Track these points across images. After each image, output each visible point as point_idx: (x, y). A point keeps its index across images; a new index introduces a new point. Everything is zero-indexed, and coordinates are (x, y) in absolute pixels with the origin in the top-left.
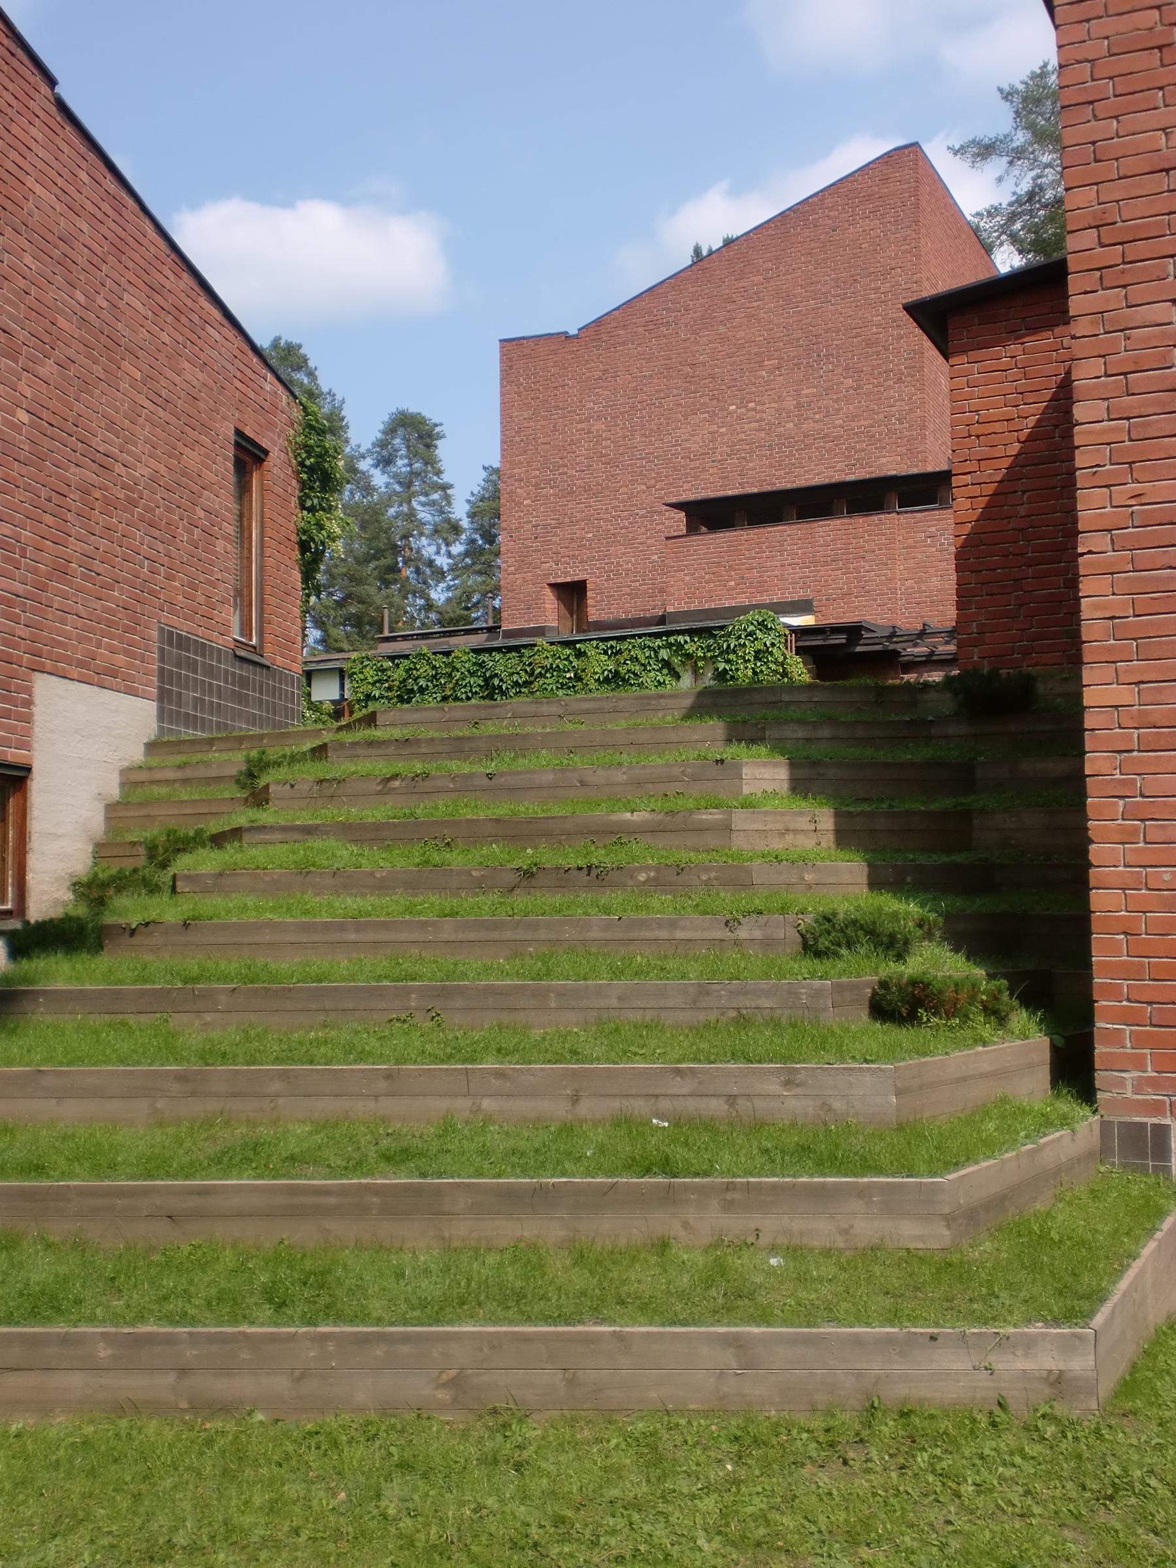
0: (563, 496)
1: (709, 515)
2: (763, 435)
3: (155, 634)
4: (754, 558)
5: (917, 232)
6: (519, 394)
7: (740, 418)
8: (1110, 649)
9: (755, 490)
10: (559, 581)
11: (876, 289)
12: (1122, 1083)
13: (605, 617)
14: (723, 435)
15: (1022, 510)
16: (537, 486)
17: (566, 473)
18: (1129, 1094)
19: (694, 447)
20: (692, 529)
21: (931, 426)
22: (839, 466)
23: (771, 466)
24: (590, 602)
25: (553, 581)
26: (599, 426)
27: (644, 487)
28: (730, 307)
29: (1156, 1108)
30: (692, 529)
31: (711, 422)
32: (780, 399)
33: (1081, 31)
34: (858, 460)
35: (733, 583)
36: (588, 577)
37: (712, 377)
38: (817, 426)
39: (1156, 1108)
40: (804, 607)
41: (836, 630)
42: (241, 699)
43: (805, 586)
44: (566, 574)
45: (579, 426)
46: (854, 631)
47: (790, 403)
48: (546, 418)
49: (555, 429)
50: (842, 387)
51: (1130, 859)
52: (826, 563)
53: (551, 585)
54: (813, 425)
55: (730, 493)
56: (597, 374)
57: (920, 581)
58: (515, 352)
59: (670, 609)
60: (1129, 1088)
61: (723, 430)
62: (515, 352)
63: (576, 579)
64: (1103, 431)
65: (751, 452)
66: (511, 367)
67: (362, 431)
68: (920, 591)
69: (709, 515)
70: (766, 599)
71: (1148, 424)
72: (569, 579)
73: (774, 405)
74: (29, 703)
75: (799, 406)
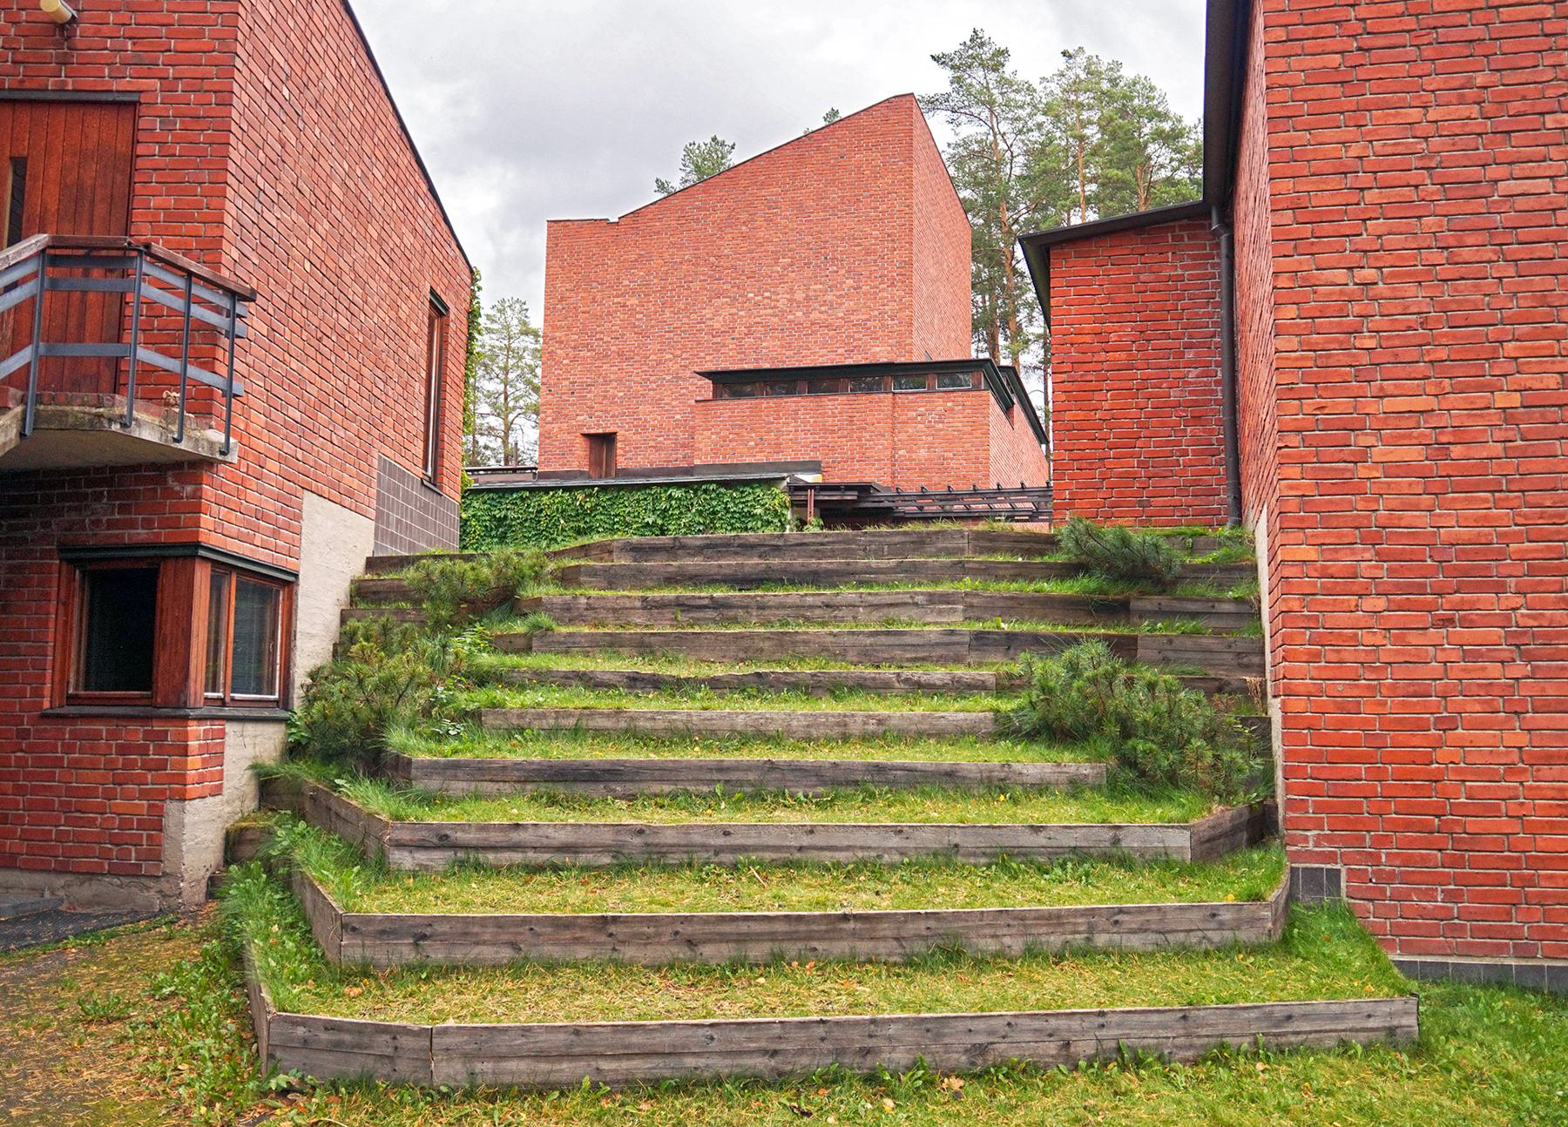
1: (731, 383)
2: (776, 320)
3: (376, 462)
5: (911, 165)
6: (563, 268)
7: (757, 304)
8: (1302, 519)
9: (767, 366)
12: (1306, 839)
13: (632, 465)
15: (1106, 405)
16: (574, 348)
18: (1311, 846)
19: (717, 326)
20: (717, 395)
21: (916, 324)
22: (840, 351)
23: (782, 347)
24: (619, 452)
25: (586, 431)
26: (634, 301)
29: (1331, 857)
30: (717, 395)
31: (731, 305)
33: (1281, 64)
37: (734, 268)
39: (1331, 857)
40: (814, 467)
41: (849, 488)
42: (423, 522)
46: (864, 489)
47: (800, 296)
48: (585, 291)
49: (594, 300)
51: (1314, 674)
53: (584, 435)
55: (746, 367)
56: (633, 257)
58: (560, 232)
59: (697, 462)
60: (1311, 844)
62: (560, 232)
64: (1297, 359)
68: (911, 460)
69: (731, 383)
70: (781, 458)
71: (1329, 356)
74: (298, 518)
75: (807, 298)
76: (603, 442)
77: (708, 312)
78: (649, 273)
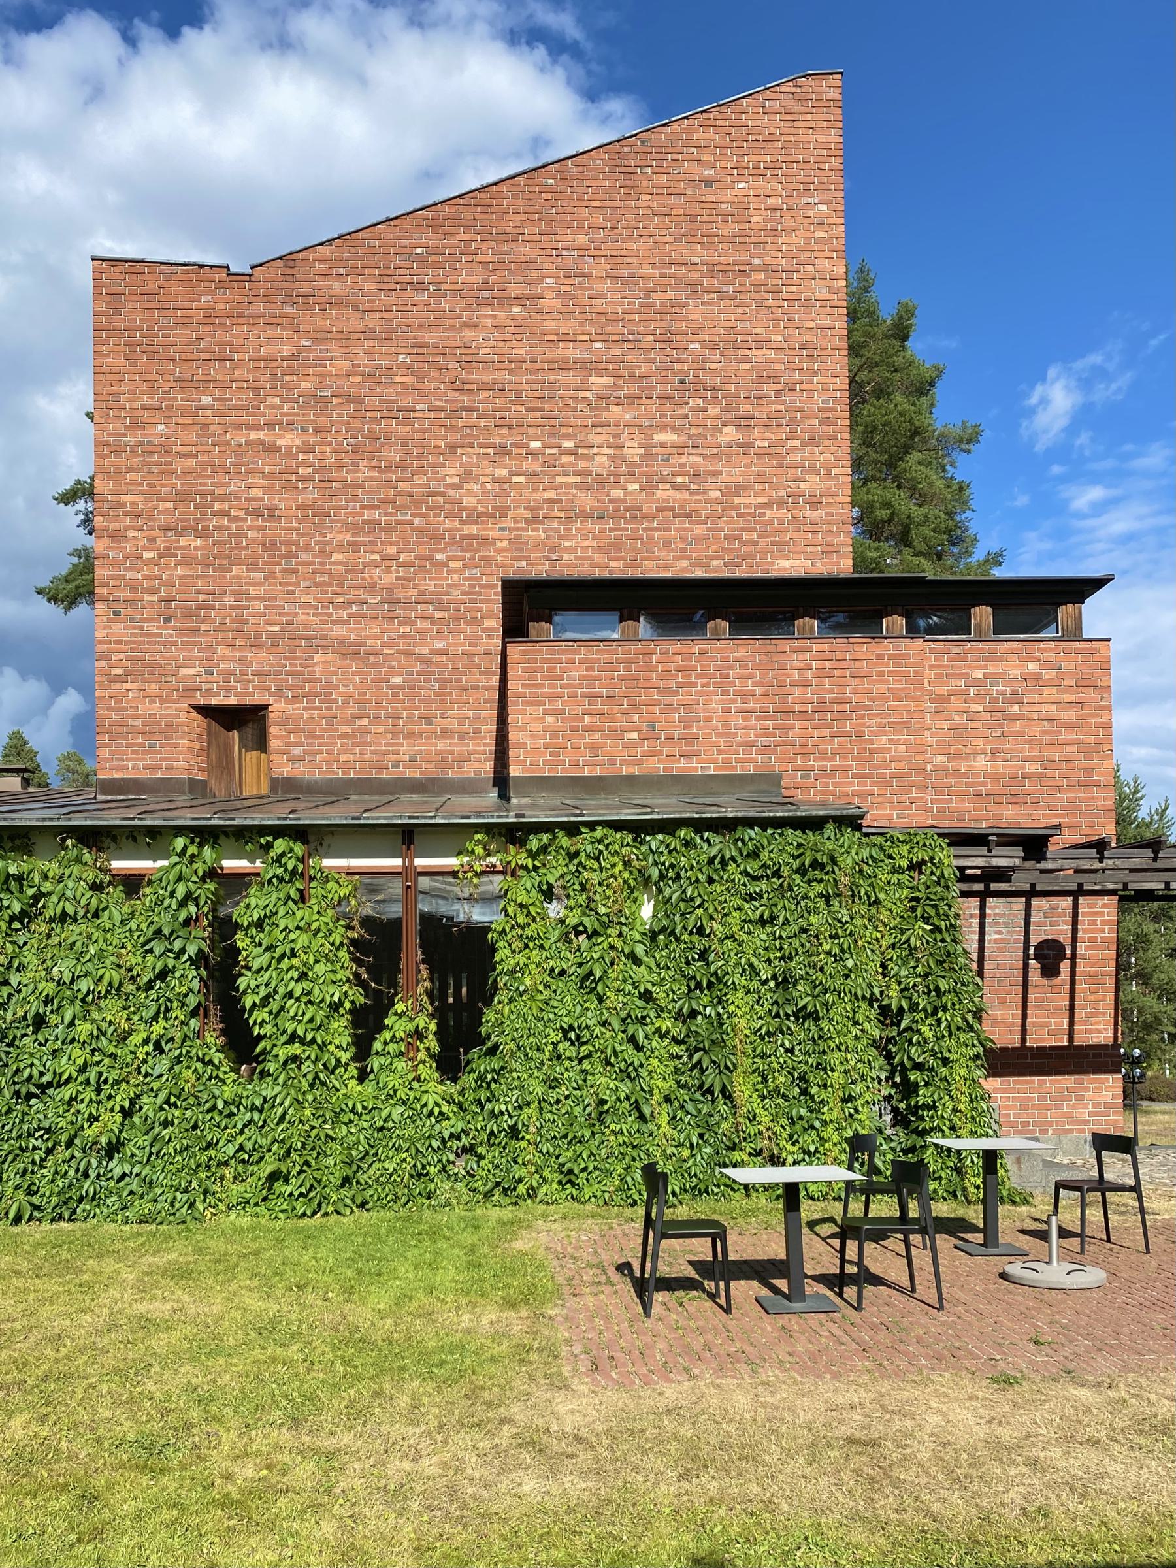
0: (221, 553)
2: (587, 497)
4: (676, 694)
10: (215, 701)
11: (776, 292)
14: (518, 487)
17: (228, 513)
23: (600, 550)
25: (201, 701)
27: (376, 557)
28: (533, 275)
32: (617, 443)
34: (744, 558)
35: (635, 735)
36: (271, 700)
38: (678, 495)
43: (765, 752)
44: (228, 690)
45: (253, 435)
50: (720, 438)
52: (803, 715)
54: (671, 492)
57: (956, 758)
61: (516, 479)
63: (248, 701)
65: (568, 523)
66: (117, 311)
67: (971, 446)
72: (233, 701)
73: (606, 450)
75: (648, 458)
76: (242, 721)
77: (451, 474)
78: (321, 384)
